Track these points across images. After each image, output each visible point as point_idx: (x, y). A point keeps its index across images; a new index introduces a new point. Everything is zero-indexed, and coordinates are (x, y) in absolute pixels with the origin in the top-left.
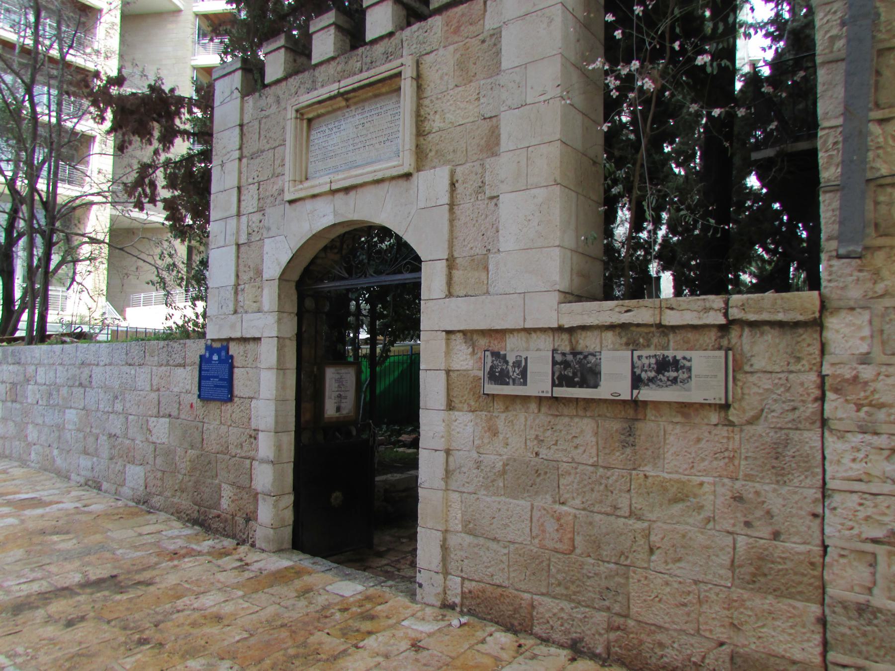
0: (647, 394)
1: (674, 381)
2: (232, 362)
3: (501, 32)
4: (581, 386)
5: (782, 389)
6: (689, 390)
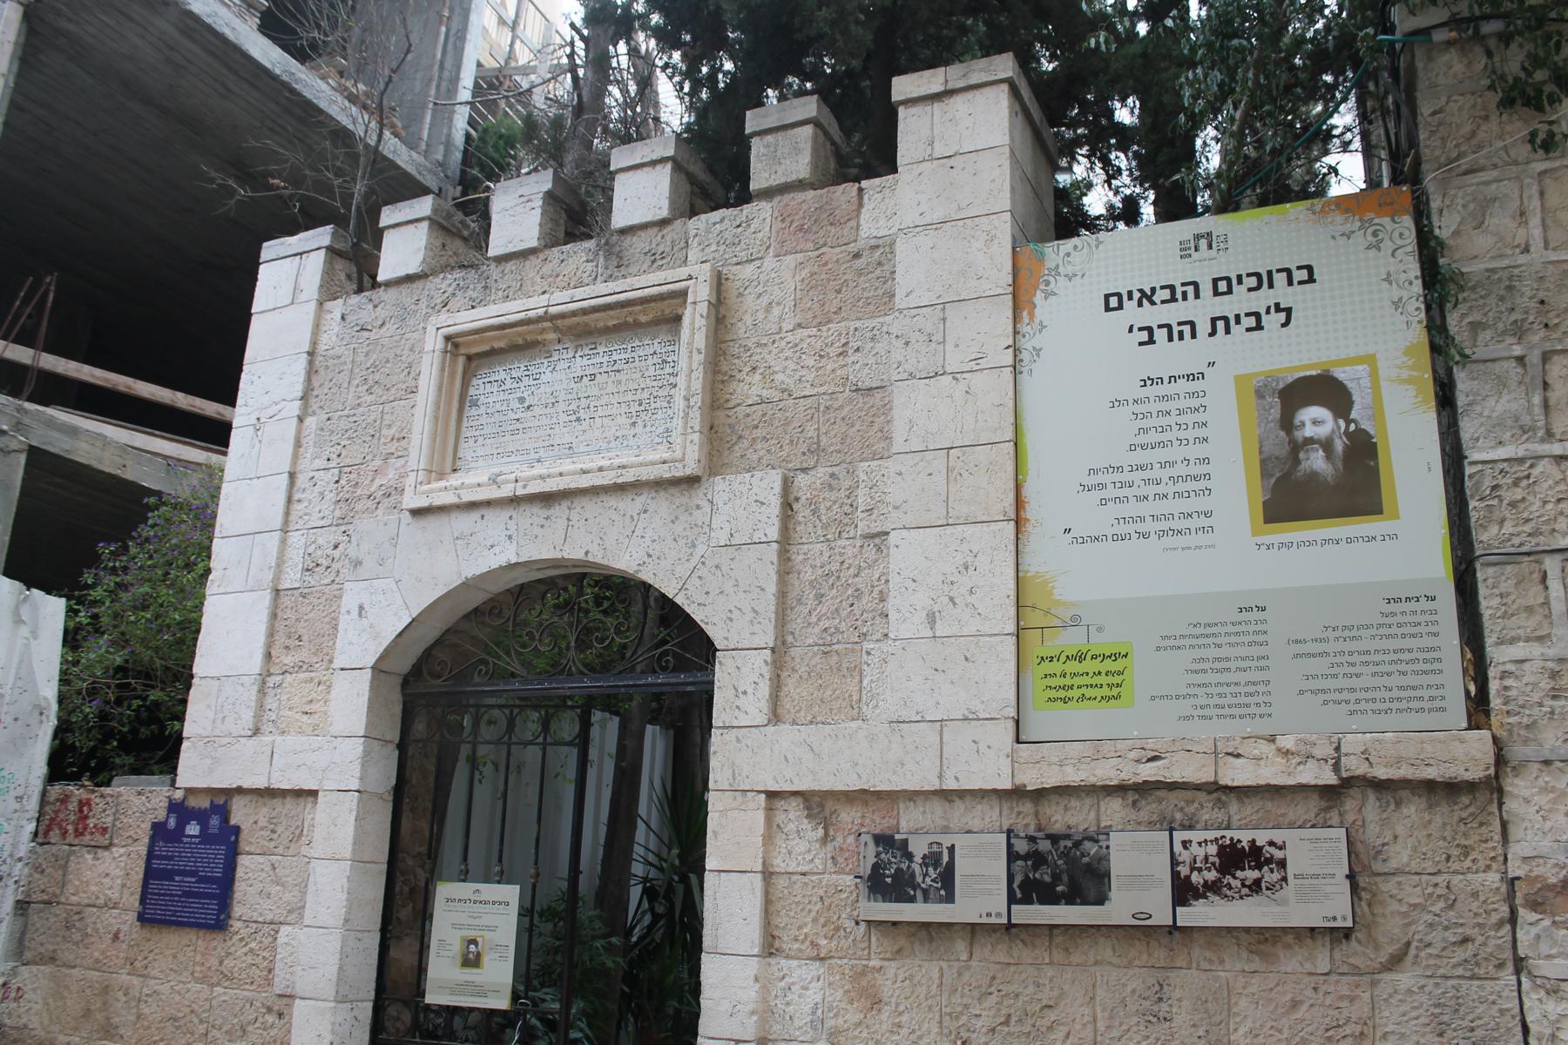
0: (1198, 914)
1: (1256, 887)
2: (237, 841)
3: (892, 244)
4: (1070, 901)
5: (1441, 904)
6: (1284, 902)
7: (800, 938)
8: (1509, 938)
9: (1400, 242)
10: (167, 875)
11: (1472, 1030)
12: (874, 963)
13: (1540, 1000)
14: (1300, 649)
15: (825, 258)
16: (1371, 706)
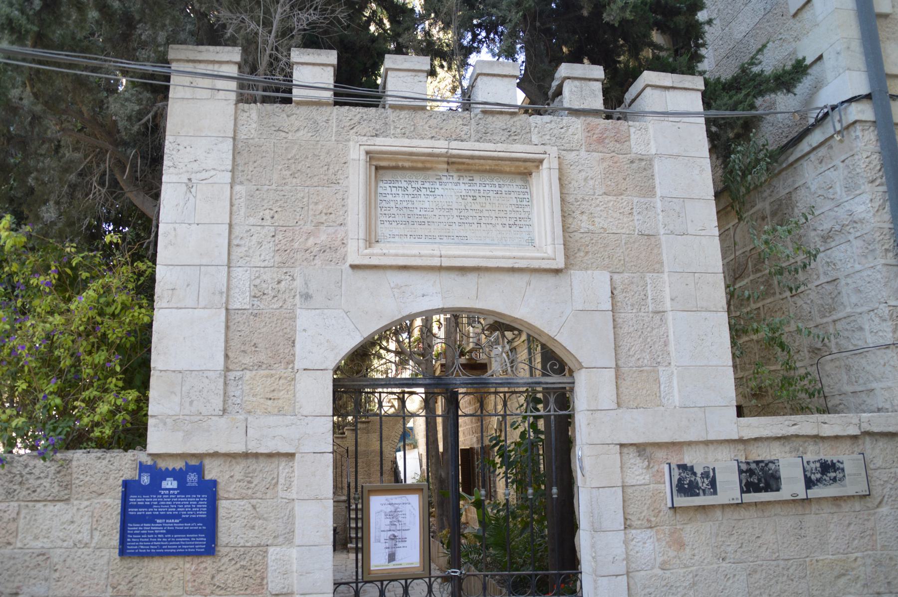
1: (834, 480)
4: (766, 491)
6: (844, 486)
7: (642, 518)
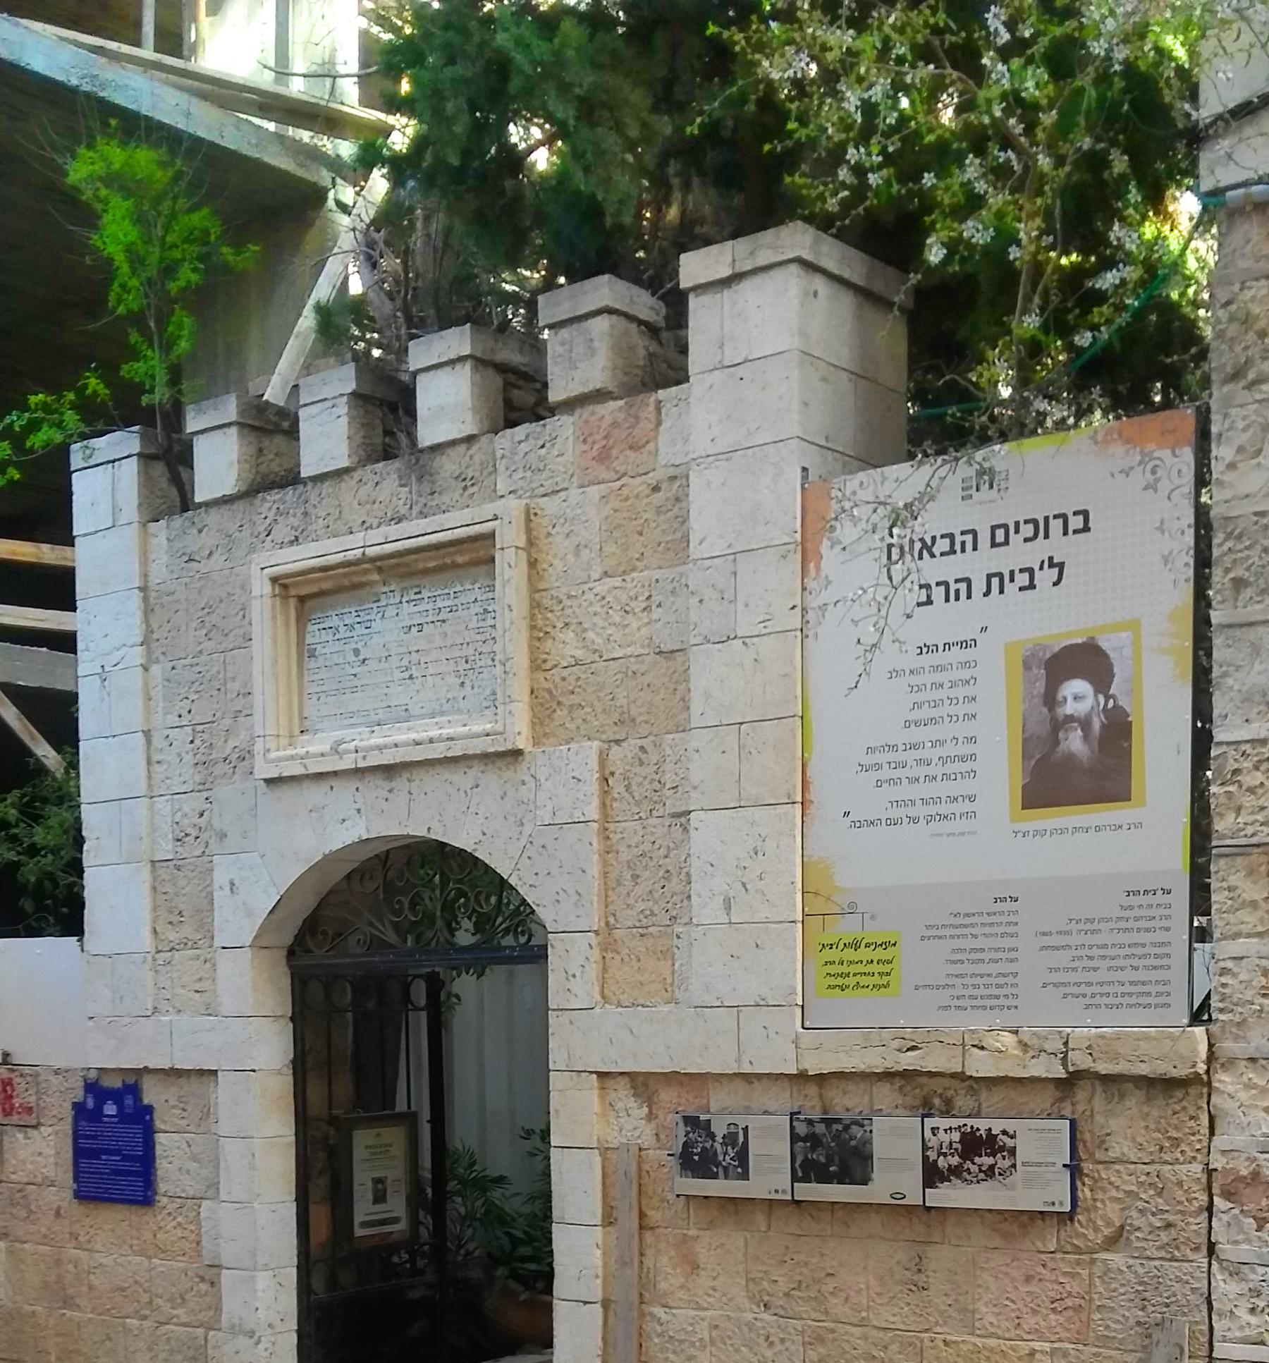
0: (948, 1195)
1: (990, 1172)
2: (152, 1119)
6: (1011, 1188)
8: (1205, 1224)
9: (1177, 482)
10: (94, 1154)
11: (1167, 1306)
12: (693, 1232)
13: (1224, 1281)
14: (1046, 941)
15: (625, 491)
16: (1105, 1000)
